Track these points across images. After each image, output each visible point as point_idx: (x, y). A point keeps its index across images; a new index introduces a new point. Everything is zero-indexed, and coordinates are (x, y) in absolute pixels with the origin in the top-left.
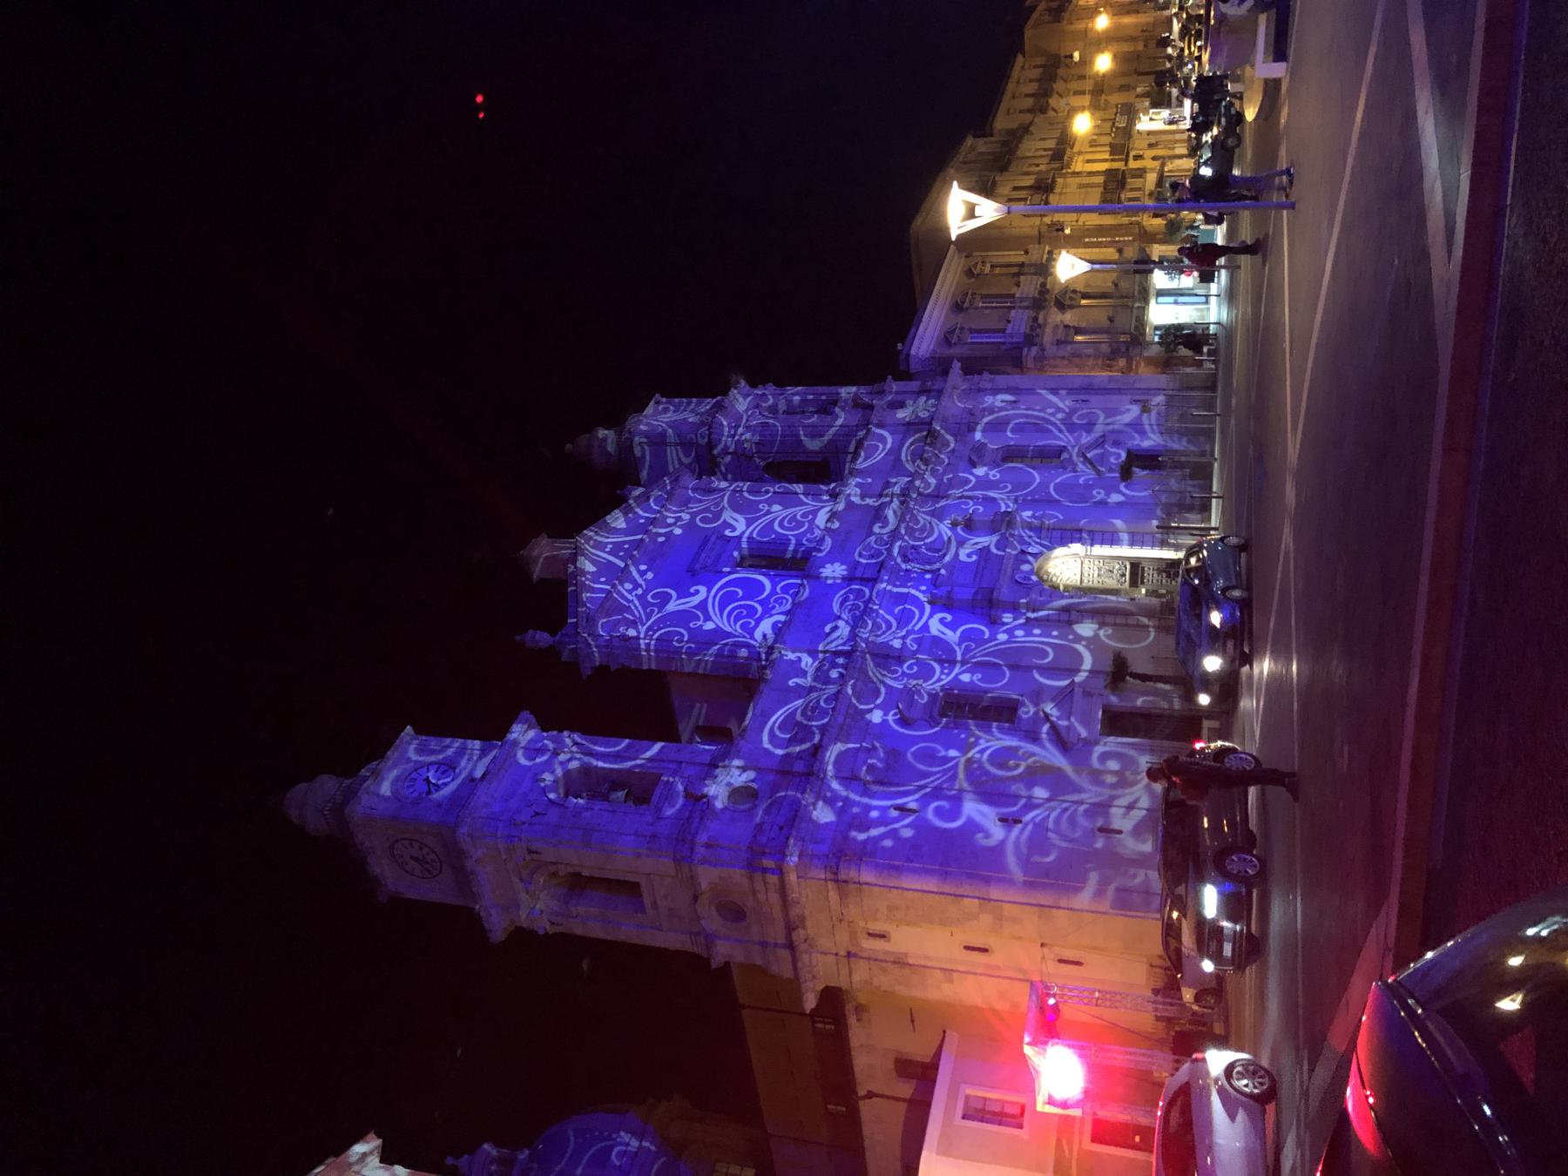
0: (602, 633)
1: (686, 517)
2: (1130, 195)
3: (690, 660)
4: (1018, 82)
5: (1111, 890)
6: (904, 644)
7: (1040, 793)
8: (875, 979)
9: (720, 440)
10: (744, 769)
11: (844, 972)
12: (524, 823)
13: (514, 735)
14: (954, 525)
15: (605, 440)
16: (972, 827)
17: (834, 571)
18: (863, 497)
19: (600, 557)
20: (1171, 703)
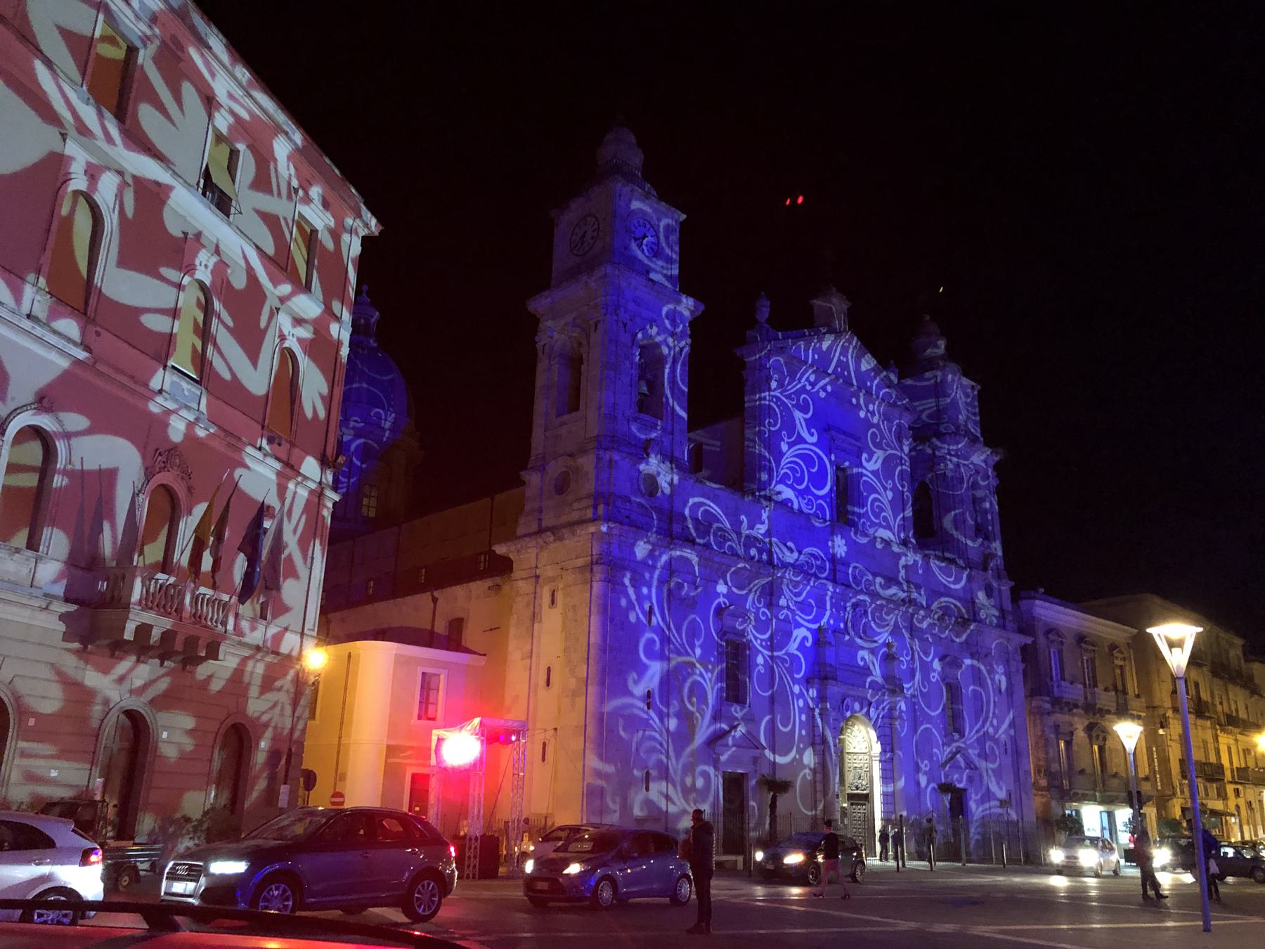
5: (600, 782)
6: (783, 608)
7: (673, 724)
9: (945, 443)
10: (671, 484)
11: (524, 574)
12: (617, 316)
13: (684, 300)
15: (937, 347)
16: (642, 670)
17: (839, 546)
18: (906, 567)
19: (836, 351)
20: (755, 829)
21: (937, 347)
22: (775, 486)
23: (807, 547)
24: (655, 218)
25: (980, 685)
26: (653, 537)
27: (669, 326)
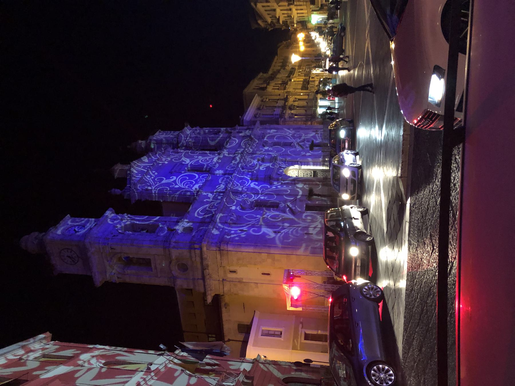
0: (139, 188)
1: (169, 159)
2: (311, 86)
3: (170, 196)
4: (276, 63)
5: (310, 248)
6: (242, 189)
7: (286, 225)
8: (232, 289)
9: (181, 141)
10: (188, 222)
11: (221, 287)
12: (109, 239)
13: (107, 214)
14: (258, 160)
15: (141, 143)
16: (264, 234)
18: (229, 154)
20: (327, 202)
21: (141, 143)
22: (193, 190)
23: (219, 182)
24: (66, 226)
25: (275, 136)
26: (210, 227)
27: (118, 221)
